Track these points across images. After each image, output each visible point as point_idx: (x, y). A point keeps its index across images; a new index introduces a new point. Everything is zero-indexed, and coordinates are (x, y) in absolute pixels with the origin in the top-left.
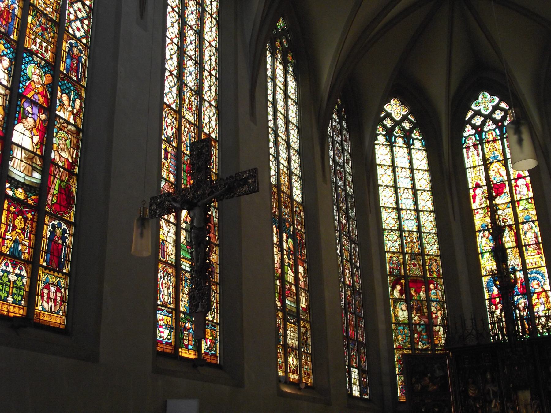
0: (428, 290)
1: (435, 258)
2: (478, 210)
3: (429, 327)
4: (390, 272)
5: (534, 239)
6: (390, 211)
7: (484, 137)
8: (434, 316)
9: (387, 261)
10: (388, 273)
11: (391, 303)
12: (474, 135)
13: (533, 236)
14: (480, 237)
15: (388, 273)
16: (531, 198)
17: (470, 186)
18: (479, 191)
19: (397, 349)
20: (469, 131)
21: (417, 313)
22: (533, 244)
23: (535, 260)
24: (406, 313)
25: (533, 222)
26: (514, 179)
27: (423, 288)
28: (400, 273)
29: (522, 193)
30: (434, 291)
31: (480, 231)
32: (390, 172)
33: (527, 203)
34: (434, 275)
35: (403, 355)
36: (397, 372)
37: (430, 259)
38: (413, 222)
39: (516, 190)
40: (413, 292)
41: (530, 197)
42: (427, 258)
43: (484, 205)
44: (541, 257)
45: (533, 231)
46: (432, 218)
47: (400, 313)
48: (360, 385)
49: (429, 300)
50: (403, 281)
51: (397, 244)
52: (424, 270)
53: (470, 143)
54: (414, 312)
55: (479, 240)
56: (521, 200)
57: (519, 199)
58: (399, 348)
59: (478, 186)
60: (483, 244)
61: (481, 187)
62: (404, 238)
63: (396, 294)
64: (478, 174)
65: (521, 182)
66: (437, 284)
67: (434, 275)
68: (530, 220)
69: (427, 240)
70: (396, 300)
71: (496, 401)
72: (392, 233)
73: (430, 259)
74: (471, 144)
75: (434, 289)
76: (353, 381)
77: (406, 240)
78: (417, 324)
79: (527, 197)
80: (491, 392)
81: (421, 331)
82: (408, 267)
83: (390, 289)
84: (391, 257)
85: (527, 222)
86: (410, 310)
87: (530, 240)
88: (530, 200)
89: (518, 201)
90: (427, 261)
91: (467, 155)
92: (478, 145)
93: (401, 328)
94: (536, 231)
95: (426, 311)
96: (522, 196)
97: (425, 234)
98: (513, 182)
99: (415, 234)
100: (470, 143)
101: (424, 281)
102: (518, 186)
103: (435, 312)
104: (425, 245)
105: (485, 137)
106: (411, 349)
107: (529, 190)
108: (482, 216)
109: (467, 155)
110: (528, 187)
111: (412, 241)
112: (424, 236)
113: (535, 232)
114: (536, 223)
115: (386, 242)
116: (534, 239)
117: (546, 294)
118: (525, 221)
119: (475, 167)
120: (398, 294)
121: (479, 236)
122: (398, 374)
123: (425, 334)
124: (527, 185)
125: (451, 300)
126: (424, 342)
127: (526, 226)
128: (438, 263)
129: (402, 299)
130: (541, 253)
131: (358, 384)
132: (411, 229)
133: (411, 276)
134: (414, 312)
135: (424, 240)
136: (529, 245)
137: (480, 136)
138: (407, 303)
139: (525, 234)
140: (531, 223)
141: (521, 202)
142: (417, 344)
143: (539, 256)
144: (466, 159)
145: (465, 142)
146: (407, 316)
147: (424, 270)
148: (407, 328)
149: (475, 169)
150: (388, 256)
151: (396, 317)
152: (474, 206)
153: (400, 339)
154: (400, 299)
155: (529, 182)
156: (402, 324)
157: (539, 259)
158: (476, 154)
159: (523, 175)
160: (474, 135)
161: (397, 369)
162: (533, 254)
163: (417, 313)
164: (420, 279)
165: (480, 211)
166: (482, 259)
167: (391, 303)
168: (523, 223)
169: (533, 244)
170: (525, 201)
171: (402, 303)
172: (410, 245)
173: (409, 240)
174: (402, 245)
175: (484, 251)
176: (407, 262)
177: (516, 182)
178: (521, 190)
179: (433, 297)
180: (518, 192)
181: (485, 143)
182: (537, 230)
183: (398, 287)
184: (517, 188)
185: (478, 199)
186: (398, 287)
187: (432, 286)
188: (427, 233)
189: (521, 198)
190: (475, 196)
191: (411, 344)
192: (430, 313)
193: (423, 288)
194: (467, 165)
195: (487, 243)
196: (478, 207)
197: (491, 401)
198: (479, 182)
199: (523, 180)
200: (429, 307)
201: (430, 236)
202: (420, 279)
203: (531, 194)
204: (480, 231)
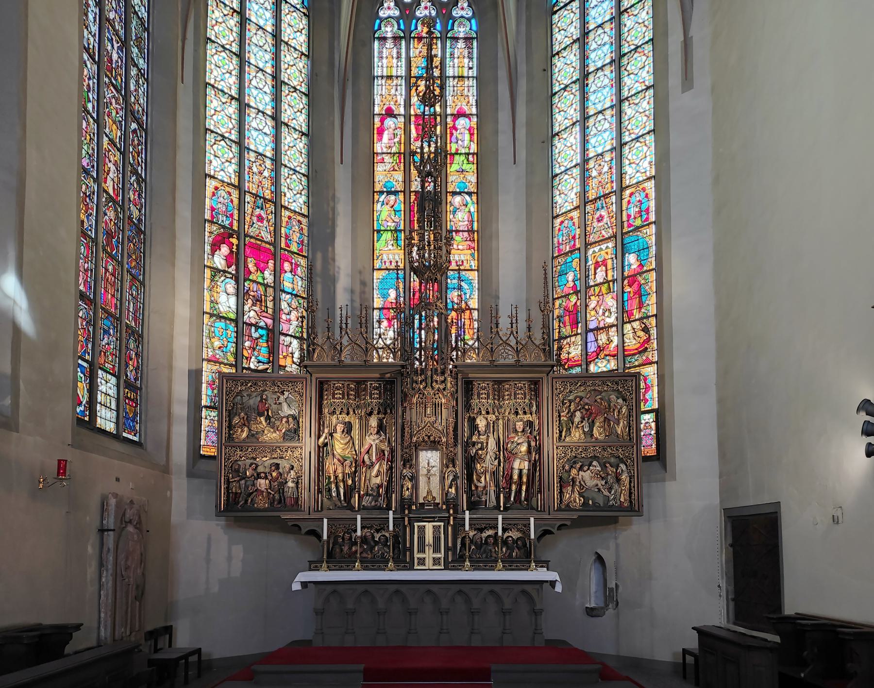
0: (278, 273)
1: (299, 218)
2: (384, 156)
3: (273, 335)
4: (212, 217)
5: (466, 223)
6: (224, 100)
7: (413, 28)
8: (284, 317)
9: (208, 193)
10: (207, 216)
11: (208, 272)
12: (397, 19)
13: (466, 219)
14: (379, 204)
15: (207, 216)
16: (473, 154)
17: (377, 110)
18: (389, 122)
19: (209, 361)
20: (389, 8)
21: (254, 305)
22: (463, 231)
23: (462, 258)
24: (233, 300)
25: (470, 194)
26: (452, 115)
27: (271, 264)
28: (231, 224)
29: (460, 142)
30: (288, 275)
31: (382, 192)
32: (232, 109)
33: (465, 161)
34: (294, 248)
35: (222, 376)
36: (204, 403)
37: (290, 218)
38: (268, 139)
39: (452, 134)
40: (251, 266)
41: (472, 151)
42: (285, 213)
43: (394, 150)
44: (472, 255)
45: (467, 210)
46: (302, 145)
47: (223, 298)
48: (118, 411)
49: (277, 287)
50: (234, 241)
51: (232, 168)
52: (276, 232)
53: (389, 31)
54: (250, 301)
55: (378, 207)
56: (457, 153)
57: (453, 151)
58: (213, 360)
59: (390, 113)
60: (384, 215)
61: (395, 116)
62: (247, 162)
63: (219, 261)
64: (393, 91)
65: (462, 122)
66: (297, 265)
67: (294, 248)
68: (466, 190)
69: (288, 180)
70: (216, 271)
71: (380, 465)
72: (222, 143)
73: (290, 218)
74: (389, 35)
75: (291, 272)
76: (100, 398)
77: (250, 168)
78: (251, 325)
79: (467, 151)
80: (374, 450)
81: (257, 339)
82: (248, 219)
83: (208, 248)
84: (216, 188)
85: (460, 193)
86: (241, 295)
87: (461, 223)
88: (470, 157)
89: (452, 155)
90: (285, 220)
91: (380, 52)
92: (401, 38)
93: (220, 324)
94: (472, 210)
95: (270, 305)
96: (460, 148)
97: (286, 170)
98: (449, 119)
99: (268, 163)
100: (389, 31)
101: (270, 253)
102: (456, 129)
103: (286, 311)
104: (284, 189)
105: (416, 28)
106: (236, 366)
107: (471, 140)
108: (388, 167)
109: (380, 52)
110: (472, 135)
111: (261, 173)
112: (285, 172)
113: (469, 212)
114: (474, 197)
115: (209, 156)
116: (466, 223)
117: (471, 313)
118: (458, 190)
119: (390, 77)
120: (223, 262)
121: (378, 201)
122: (206, 407)
123: (265, 345)
124: (470, 129)
125: (315, 304)
126: (260, 358)
127: (458, 199)
128: (302, 229)
129: (230, 273)
130: (474, 248)
131: (113, 406)
132: (261, 150)
133: (251, 237)
134: (250, 301)
135: (283, 180)
136: (457, 231)
137: (408, 25)
138: (237, 281)
139: (454, 212)
140: (467, 197)
141: (457, 157)
142: (248, 359)
143: (469, 252)
144: (376, 60)
145: (380, 28)
146: (234, 307)
147: (276, 232)
148: (232, 327)
149: (389, 82)
150: (211, 184)
151: (214, 302)
152: (378, 148)
153: (217, 344)
154: (224, 271)
155: (475, 127)
156: (223, 317)
157: (469, 257)
158: (395, 56)
159: (468, 112)
160: (397, 19)
161: (204, 397)
162: (460, 247)
163: (254, 305)
164: (268, 246)
165: (387, 158)
166: (378, 241)
167: (208, 273)
168: (454, 193)
169: (463, 231)
170: (463, 158)
171: (228, 280)
172: (256, 178)
173: (255, 169)
174: (240, 174)
175: (382, 228)
176: (248, 208)
177: (454, 121)
178: (460, 137)
179: (287, 286)
180: (454, 139)
181: (414, 38)
182: (473, 208)
183: (225, 250)
184: (454, 131)
185: (386, 136)
186: (225, 250)
187: (287, 266)
188: (291, 169)
189: (457, 150)
190: (381, 131)
191: (236, 358)
192: (277, 310)
193: (271, 264)
194: (377, 72)
195: (389, 215)
196: (385, 150)
197: (372, 465)
198: (393, 107)
199: (467, 120)
200: (276, 301)
201: (294, 176)
202: (268, 246)
203: (474, 148)
204: (382, 192)
